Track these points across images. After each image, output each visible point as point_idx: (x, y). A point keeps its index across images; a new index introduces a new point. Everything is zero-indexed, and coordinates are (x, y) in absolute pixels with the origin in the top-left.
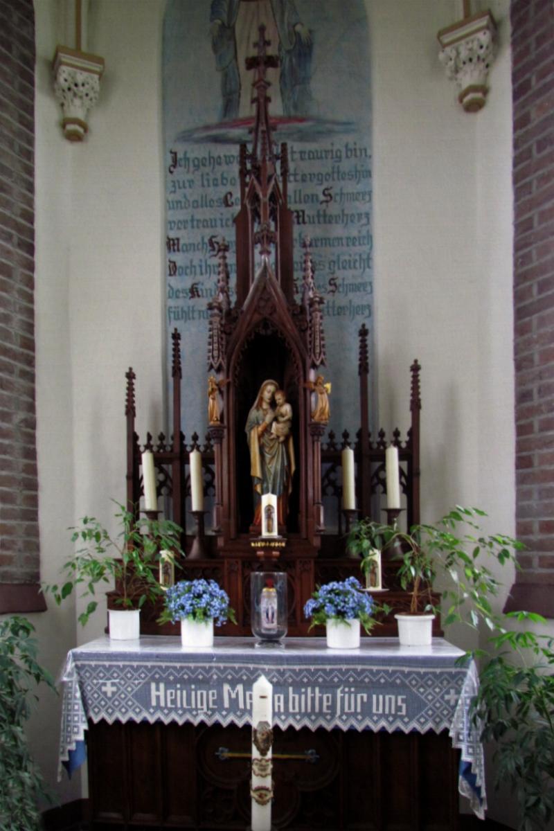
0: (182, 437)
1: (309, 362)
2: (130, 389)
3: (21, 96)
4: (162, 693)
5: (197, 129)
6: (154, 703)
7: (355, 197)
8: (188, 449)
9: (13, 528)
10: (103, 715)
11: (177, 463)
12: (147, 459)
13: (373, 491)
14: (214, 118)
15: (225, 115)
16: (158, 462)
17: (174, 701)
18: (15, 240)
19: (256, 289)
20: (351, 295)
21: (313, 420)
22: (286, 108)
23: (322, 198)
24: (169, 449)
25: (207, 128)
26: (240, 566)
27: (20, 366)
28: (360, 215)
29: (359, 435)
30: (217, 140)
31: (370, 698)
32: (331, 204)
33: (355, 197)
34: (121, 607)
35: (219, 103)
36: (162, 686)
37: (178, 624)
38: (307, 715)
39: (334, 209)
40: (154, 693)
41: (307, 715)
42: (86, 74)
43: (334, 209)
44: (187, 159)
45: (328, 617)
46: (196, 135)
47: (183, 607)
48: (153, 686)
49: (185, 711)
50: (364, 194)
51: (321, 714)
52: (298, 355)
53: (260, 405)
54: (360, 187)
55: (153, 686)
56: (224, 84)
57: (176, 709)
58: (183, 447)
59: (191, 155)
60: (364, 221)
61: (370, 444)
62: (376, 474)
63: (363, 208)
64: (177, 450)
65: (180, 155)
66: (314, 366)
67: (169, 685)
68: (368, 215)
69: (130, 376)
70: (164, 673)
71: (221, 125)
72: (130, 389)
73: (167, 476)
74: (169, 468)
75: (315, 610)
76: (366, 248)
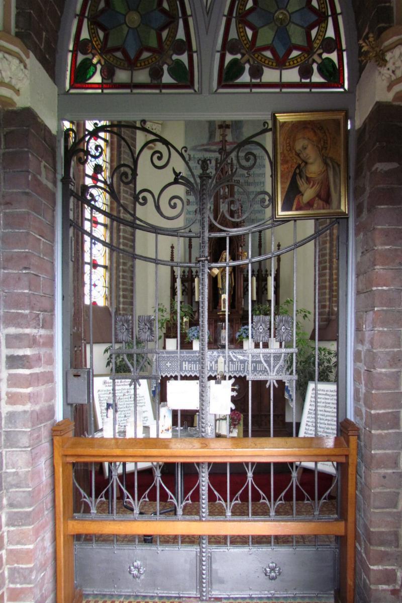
0: (192, 272)
1: (239, 245)
2: (172, 252)
3: (131, 134)
4: (187, 366)
5: (199, 146)
6: (184, 369)
7: (259, 175)
8: (194, 276)
9: (127, 308)
10: (166, 374)
11: (190, 283)
12: (179, 281)
13: (263, 293)
14: (205, 141)
15: (209, 141)
16: (183, 282)
17: (191, 368)
18: (129, 193)
19: (221, 216)
20: (257, 215)
21: (221, 200)
22: (233, 139)
23: (246, 175)
24: (186, 277)
25: (203, 145)
26: (213, 322)
27: (130, 243)
28: (261, 183)
29: (258, 271)
30: (206, 150)
31: (256, 365)
32: (250, 178)
33: (259, 175)
34: (170, 337)
35: (207, 135)
36: (187, 363)
37: (192, 341)
38: (236, 371)
39: (251, 180)
40: (184, 365)
41: (236, 371)
42: (156, 125)
43: (251, 180)
44: (194, 158)
45: (243, 338)
46: (198, 148)
47: (194, 335)
48: (184, 363)
49: (195, 371)
50: (262, 174)
51: (240, 371)
52: (236, 243)
53: (221, 260)
54: (261, 172)
55: (184, 363)
56: (209, 128)
57: (191, 371)
58: (192, 276)
59: (196, 156)
60: (262, 185)
61: (262, 275)
62: (264, 287)
63: (262, 180)
64: (190, 277)
65: (192, 156)
66: (241, 246)
67: (189, 362)
68: (264, 183)
69: (172, 247)
70: (283, 209)
71: (208, 144)
72: (172, 252)
73: (186, 287)
74: (186, 284)
75: (239, 336)
76: (263, 179)
